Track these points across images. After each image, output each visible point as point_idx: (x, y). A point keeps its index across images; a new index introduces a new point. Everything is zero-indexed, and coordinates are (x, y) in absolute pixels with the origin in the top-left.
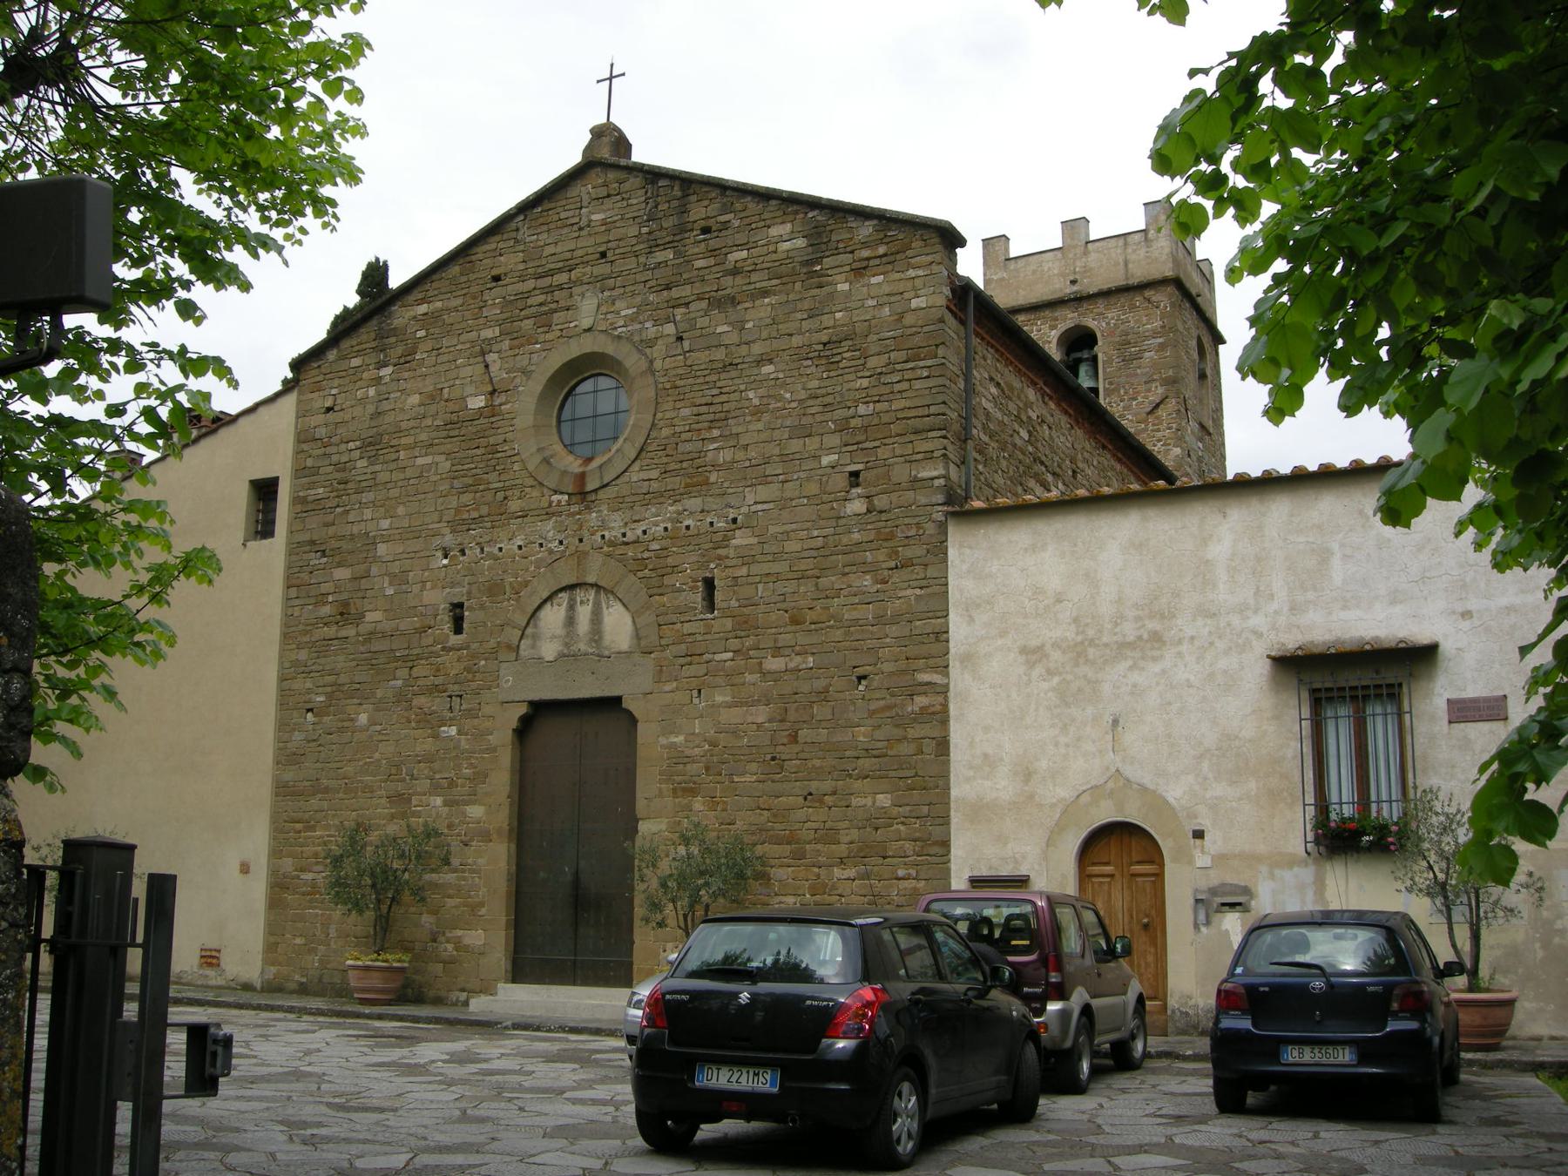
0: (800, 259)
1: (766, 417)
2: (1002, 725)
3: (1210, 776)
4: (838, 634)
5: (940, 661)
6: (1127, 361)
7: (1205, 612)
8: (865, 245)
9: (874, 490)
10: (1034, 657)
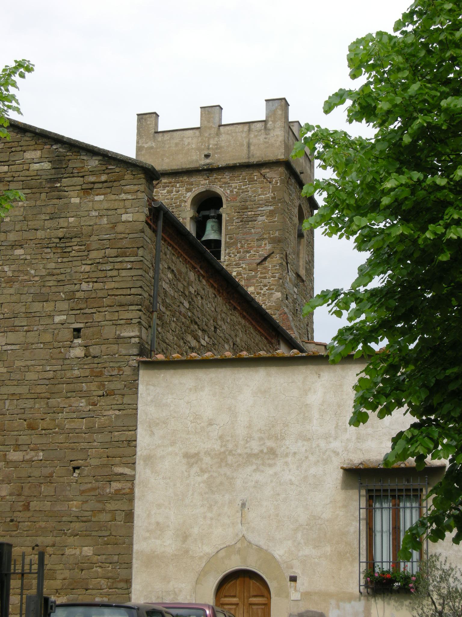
0: (46, 177)
1: (16, 285)
2: (170, 504)
3: (302, 541)
4: (61, 438)
5: (129, 460)
6: (245, 221)
7: (304, 438)
8: (92, 173)
9: (90, 342)
10: (193, 460)
